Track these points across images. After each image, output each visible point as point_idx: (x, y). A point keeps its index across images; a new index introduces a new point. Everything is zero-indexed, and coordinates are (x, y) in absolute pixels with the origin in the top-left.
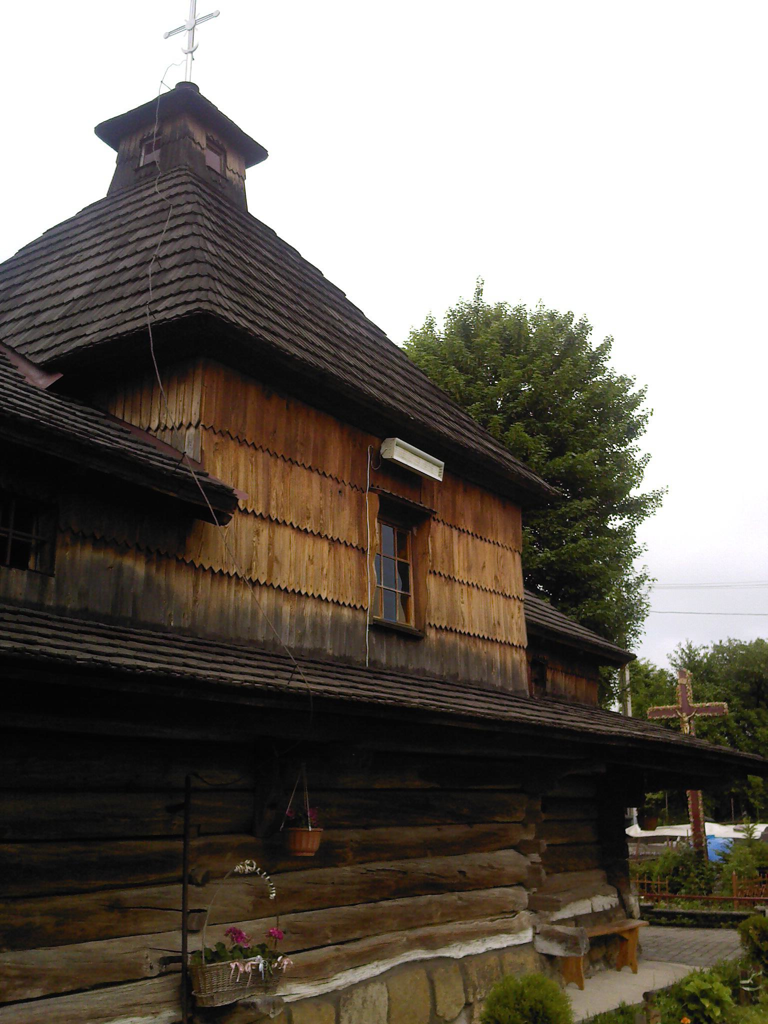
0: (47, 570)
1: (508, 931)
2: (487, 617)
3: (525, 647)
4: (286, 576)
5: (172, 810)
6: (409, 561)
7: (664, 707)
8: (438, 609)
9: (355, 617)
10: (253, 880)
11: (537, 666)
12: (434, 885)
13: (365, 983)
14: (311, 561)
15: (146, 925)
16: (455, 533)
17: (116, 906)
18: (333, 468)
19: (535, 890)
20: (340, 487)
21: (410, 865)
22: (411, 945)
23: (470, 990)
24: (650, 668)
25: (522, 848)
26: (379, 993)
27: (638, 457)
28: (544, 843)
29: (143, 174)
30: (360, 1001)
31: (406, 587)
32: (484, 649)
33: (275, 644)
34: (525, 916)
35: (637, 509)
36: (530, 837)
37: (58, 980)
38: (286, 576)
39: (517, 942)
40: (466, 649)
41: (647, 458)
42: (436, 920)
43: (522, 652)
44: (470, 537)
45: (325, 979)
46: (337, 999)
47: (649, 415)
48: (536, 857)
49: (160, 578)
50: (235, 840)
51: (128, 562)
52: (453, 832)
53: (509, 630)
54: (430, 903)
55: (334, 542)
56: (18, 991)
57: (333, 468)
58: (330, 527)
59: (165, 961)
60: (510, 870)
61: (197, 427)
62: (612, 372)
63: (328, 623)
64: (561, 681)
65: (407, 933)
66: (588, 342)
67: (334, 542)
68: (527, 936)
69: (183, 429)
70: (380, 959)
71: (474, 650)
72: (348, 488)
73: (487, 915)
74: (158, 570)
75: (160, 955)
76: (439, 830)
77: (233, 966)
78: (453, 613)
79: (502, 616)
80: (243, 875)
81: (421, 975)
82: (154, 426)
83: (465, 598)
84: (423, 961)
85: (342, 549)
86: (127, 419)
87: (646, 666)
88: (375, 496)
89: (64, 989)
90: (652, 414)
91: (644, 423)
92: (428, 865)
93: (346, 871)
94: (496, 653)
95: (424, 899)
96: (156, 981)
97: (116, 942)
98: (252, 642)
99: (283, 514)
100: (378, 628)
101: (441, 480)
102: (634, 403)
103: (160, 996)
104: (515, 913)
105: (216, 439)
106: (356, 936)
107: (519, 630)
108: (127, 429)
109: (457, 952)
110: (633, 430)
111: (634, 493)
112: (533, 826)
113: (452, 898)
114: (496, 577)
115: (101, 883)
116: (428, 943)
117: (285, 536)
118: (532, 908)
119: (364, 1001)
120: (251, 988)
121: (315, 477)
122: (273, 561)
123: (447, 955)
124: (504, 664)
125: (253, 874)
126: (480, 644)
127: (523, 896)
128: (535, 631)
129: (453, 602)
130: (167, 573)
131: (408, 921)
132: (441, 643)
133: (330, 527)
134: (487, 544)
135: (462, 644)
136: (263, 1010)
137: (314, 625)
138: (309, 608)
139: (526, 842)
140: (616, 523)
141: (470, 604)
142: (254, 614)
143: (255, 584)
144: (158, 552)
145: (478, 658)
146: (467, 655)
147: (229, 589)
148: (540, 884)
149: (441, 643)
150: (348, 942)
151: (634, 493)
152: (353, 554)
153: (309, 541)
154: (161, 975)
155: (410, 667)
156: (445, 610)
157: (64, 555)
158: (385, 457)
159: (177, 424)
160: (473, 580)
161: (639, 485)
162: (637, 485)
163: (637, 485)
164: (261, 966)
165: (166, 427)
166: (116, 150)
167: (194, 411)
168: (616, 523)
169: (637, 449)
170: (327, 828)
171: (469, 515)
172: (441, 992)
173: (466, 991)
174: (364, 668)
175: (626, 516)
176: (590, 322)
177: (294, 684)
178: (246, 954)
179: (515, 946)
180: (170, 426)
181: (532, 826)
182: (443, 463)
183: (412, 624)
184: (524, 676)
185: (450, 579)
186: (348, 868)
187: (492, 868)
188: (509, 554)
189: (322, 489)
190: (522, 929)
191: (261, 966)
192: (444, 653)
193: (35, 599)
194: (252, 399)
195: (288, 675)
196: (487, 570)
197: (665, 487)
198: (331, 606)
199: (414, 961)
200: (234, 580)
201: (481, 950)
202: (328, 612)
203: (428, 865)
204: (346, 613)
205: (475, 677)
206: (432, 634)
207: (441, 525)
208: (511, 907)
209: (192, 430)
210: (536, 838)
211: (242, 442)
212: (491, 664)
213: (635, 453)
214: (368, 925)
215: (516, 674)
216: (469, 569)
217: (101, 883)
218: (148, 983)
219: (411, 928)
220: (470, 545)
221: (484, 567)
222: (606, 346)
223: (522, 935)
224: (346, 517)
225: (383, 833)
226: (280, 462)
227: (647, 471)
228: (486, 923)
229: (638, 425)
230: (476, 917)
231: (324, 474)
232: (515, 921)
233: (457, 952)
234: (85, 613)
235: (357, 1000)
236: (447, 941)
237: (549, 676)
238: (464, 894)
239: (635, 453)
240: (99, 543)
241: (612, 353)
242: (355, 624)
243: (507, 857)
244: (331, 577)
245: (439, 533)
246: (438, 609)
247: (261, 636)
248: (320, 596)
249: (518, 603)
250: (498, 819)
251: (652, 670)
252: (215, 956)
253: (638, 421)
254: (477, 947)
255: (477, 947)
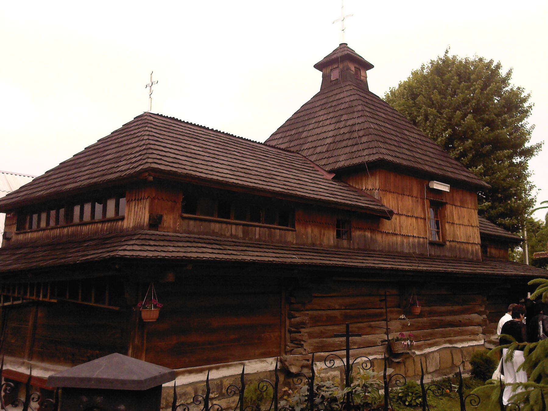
0: (350, 238)
1: (476, 340)
2: (466, 234)
3: (480, 243)
4: (404, 231)
5: (381, 301)
6: (439, 219)
7: (541, 252)
8: (449, 234)
9: (424, 241)
10: (403, 321)
11: (484, 246)
12: (451, 324)
13: (433, 352)
14: (411, 225)
15: (377, 332)
16: (454, 207)
17: (370, 326)
18: (415, 193)
19: (485, 327)
20: (417, 199)
21: (443, 318)
22: (445, 342)
23: (464, 357)
24: (540, 223)
25: (480, 313)
26: (437, 355)
27: (528, 127)
28: (488, 312)
29: (334, 83)
30: (432, 357)
31: (438, 228)
32: (465, 246)
33: (403, 252)
34: (481, 335)
35: (529, 153)
36: (483, 309)
37: (360, 344)
38: (404, 231)
39: (479, 344)
40: (459, 247)
41: (533, 127)
42: (452, 336)
43: (479, 246)
44: (459, 207)
45: (422, 350)
46: (426, 356)
47: (532, 106)
48: (485, 316)
49: (374, 237)
50: (396, 309)
51: (366, 233)
52: (456, 308)
53: (474, 238)
54: (450, 330)
55: (417, 218)
56: (352, 346)
57: (415, 193)
58: (415, 213)
59: (382, 341)
60: (476, 320)
61: (378, 190)
62: (513, 86)
63: (416, 244)
64: (493, 251)
65: (444, 339)
66: (500, 73)
67: (417, 218)
68: (482, 342)
69: (374, 191)
70: (436, 346)
71: (462, 247)
72: (419, 199)
73: (468, 335)
74: (373, 234)
75: (381, 340)
76: (452, 307)
77: (402, 342)
78: (454, 235)
79: (471, 233)
80: (401, 319)
81: (449, 352)
82: (364, 188)
83: (458, 230)
84: (449, 347)
85: (419, 219)
86: (354, 186)
87: (538, 222)
88: (428, 201)
89: (361, 347)
90: (534, 105)
91: (530, 110)
92: (449, 318)
93: (425, 319)
94: (470, 247)
95: (447, 329)
96: (381, 346)
97: (370, 336)
98: (397, 252)
99: (402, 212)
100: (432, 243)
101: (449, 191)
102: (524, 100)
103: (382, 350)
104: (478, 334)
105: (384, 193)
106: (429, 339)
107: (478, 237)
108: (361, 193)
109: (460, 345)
110: (525, 113)
111: (527, 145)
112: (484, 306)
113: (457, 329)
114: (469, 220)
115: (367, 320)
116: (450, 342)
117: (403, 218)
118: (483, 333)
119: (433, 357)
120: (406, 349)
121: (410, 197)
122: (401, 226)
123: (456, 346)
124: (472, 250)
125: (404, 319)
126: (464, 244)
127: (481, 329)
128: (484, 237)
129: (454, 231)
130: (376, 235)
131: (444, 335)
132: (451, 246)
133: (415, 213)
134: (465, 209)
135: (458, 246)
136: (411, 354)
137: (413, 245)
138: (411, 239)
139: (481, 311)
140: (517, 160)
141: (460, 231)
142: (397, 244)
143: (396, 234)
144: (373, 229)
145: (464, 249)
146: (459, 248)
147: (390, 238)
148: (486, 325)
149: (451, 246)
150: (426, 340)
151: (527, 145)
152: (422, 221)
153: (410, 219)
154: (381, 345)
155: (441, 255)
156: (452, 234)
157: (353, 234)
158: (431, 187)
159: (372, 189)
160: (461, 223)
161: (529, 141)
162: (528, 141)
163: (528, 141)
164: (409, 343)
165: (368, 189)
166: (322, 71)
167: (377, 185)
168: (517, 160)
169: (527, 123)
170: (422, 306)
171: (458, 199)
172: (455, 357)
173: (462, 358)
174: (427, 257)
175: (523, 157)
176: (502, 64)
177: (419, 268)
178: (405, 340)
179: (478, 345)
180: (369, 189)
181: (484, 306)
182: (449, 185)
183: (441, 240)
184: (480, 254)
185: (453, 223)
186: (426, 319)
187: (470, 319)
188: (473, 211)
189: (412, 201)
190: (480, 340)
191: (409, 343)
192: (452, 249)
193: (348, 247)
194: (392, 178)
195: (417, 265)
196: (465, 218)
197: (542, 141)
198: (417, 238)
199: (446, 347)
200: (391, 234)
201: (467, 345)
202: (416, 240)
203: (449, 318)
204: (421, 240)
205: (462, 256)
206: (448, 243)
207: (449, 205)
208: (476, 333)
209: (377, 191)
210: (485, 310)
211: (390, 192)
212: (468, 251)
213: (526, 125)
214: (432, 335)
215: (477, 253)
216: (459, 219)
217: (367, 320)
218: (379, 347)
219: (445, 337)
220: (459, 211)
221: (464, 217)
222: (509, 74)
223: (480, 341)
224: (420, 209)
225: (435, 308)
226: (400, 195)
227: (532, 135)
228: (468, 337)
229: (527, 111)
230: (465, 335)
231: (413, 196)
232: (478, 337)
233: (460, 345)
234: (359, 249)
235: (431, 357)
236: (456, 342)
237: (488, 250)
238: (460, 328)
239: (526, 125)
240: (360, 229)
241: (513, 76)
242: (424, 243)
243: (474, 316)
244: (416, 229)
245: (449, 207)
246: (449, 234)
247: (399, 250)
248: (414, 236)
249: (477, 228)
250: (471, 303)
251: (542, 224)
252: (397, 340)
253: (527, 109)
254: (465, 345)
255: (465, 345)
